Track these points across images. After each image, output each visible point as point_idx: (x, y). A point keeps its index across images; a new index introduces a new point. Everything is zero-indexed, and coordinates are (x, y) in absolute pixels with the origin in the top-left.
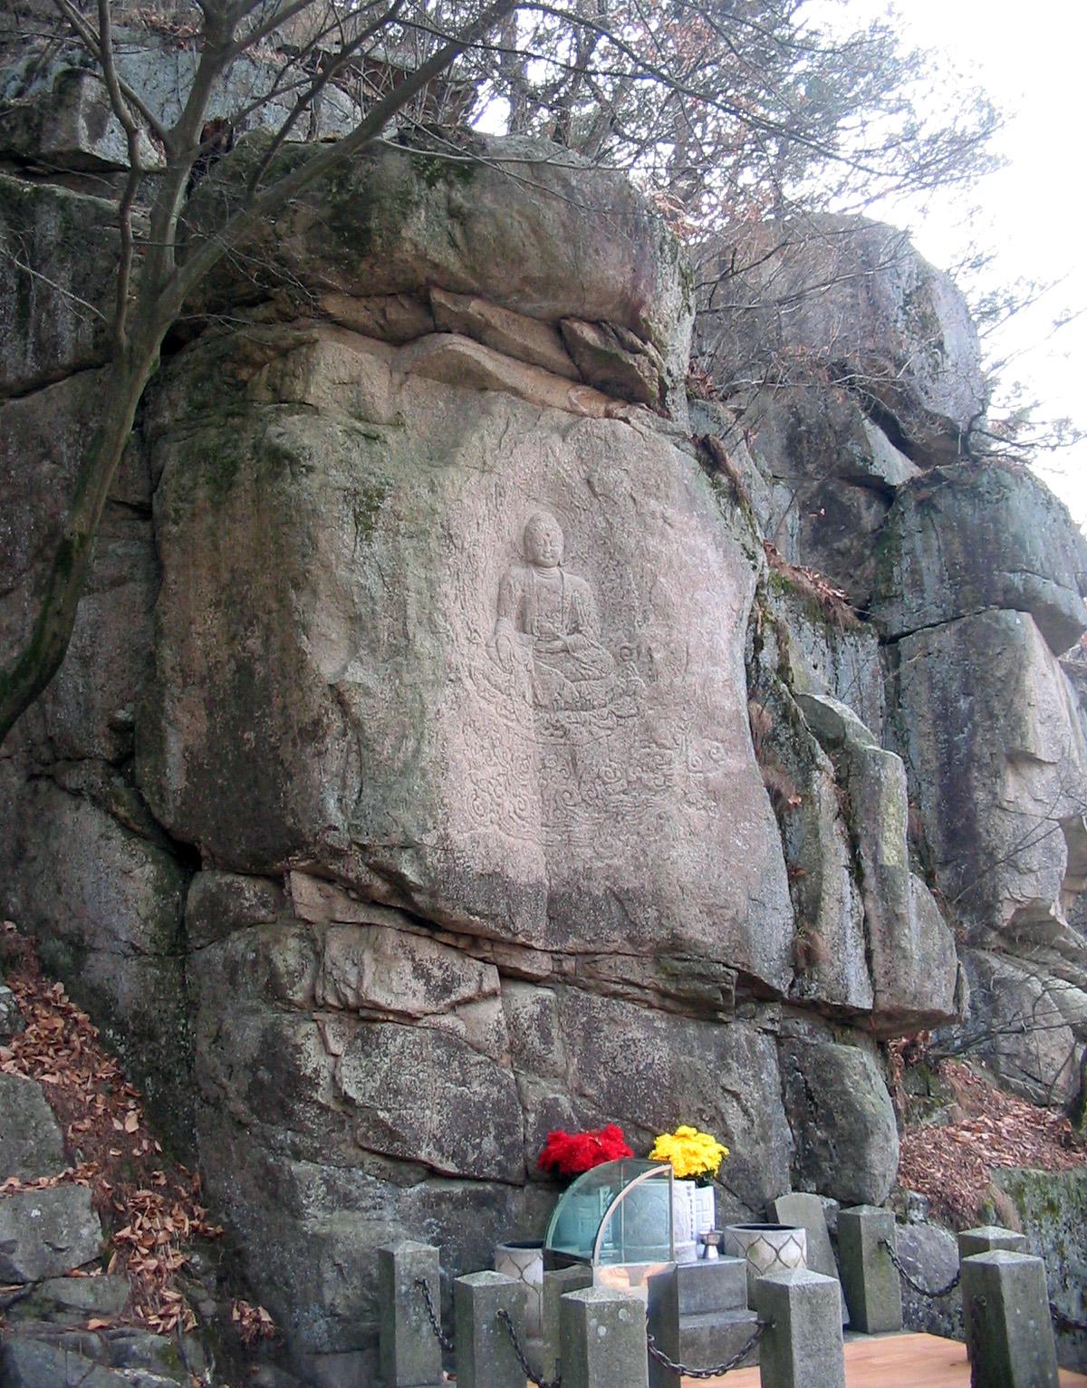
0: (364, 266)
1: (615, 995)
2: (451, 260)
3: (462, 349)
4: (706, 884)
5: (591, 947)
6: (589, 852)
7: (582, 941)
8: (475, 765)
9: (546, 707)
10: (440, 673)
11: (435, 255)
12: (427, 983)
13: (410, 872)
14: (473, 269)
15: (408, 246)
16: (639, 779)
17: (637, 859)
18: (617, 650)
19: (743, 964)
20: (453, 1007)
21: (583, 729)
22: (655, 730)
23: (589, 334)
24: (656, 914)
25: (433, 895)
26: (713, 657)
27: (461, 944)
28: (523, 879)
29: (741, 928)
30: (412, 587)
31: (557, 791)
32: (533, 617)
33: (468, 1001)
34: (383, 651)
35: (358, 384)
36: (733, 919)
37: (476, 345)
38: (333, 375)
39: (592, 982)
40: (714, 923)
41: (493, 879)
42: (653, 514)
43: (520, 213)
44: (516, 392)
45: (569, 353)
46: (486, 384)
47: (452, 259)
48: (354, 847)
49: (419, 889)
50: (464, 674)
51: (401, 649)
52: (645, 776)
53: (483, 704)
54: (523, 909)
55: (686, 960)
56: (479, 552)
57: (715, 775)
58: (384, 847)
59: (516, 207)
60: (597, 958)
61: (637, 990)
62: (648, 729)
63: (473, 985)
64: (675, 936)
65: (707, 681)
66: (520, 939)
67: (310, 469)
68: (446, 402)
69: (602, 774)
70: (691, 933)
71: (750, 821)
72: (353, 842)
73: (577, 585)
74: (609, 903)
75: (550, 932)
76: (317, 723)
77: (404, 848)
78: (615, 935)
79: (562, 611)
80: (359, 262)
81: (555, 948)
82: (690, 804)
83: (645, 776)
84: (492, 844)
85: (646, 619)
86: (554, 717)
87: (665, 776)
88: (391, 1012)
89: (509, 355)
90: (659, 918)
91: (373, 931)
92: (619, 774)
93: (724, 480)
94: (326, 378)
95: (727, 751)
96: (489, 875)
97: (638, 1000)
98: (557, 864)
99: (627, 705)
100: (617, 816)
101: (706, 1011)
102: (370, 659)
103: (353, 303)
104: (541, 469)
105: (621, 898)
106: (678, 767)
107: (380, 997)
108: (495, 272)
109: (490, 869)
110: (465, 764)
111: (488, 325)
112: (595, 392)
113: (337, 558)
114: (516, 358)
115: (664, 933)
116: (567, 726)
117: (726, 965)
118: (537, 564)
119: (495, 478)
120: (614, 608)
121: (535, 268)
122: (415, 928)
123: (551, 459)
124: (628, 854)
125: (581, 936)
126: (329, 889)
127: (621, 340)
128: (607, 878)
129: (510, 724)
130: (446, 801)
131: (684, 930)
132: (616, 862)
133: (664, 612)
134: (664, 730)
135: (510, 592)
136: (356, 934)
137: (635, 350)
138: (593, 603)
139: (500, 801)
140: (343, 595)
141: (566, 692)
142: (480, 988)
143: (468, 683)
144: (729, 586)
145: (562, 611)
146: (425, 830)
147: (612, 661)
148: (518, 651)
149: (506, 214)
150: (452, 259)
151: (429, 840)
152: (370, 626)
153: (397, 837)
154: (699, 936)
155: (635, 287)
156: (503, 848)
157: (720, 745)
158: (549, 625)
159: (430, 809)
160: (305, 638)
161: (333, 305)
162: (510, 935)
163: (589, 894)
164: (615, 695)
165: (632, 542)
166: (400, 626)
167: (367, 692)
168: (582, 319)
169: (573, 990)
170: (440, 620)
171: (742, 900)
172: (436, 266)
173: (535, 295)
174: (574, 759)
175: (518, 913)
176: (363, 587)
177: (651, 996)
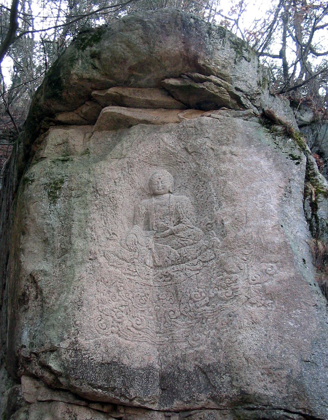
0: (64, 94)
2: (96, 75)
3: (110, 111)
4: (264, 354)
5: (187, 406)
6: (185, 345)
7: (182, 403)
8: (103, 302)
9: (161, 266)
11: (86, 75)
13: (54, 365)
14: (106, 75)
15: (74, 77)
16: (216, 295)
17: (215, 344)
18: (204, 227)
19: (304, 410)
21: (181, 273)
22: (226, 264)
23: (172, 81)
24: (229, 379)
25: (67, 377)
26: (265, 215)
27: (105, 409)
28: (137, 365)
29: (296, 382)
30: (76, 219)
31: (166, 312)
32: (153, 222)
34: (58, 253)
35: (67, 142)
36: (288, 376)
37: (119, 108)
38: (55, 142)
40: (274, 381)
41: (112, 367)
42: (224, 153)
43: (121, 42)
44: (146, 122)
45: (173, 97)
46: (130, 123)
47: (95, 74)
48: (33, 355)
51: (66, 250)
52: (219, 293)
53: (112, 269)
54: (136, 384)
55: (253, 409)
56: (117, 196)
57: (271, 284)
58: (43, 352)
59: (118, 40)
60: (192, 412)
62: (221, 265)
64: (243, 393)
65: (260, 230)
66: (136, 403)
67: (33, 181)
68: (112, 138)
69: (192, 297)
70: (254, 389)
71: (300, 308)
72: (31, 353)
73: (183, 200)
74: (197, 376)
75: (163, 399)
76: (24, 294)
77: (52, 351)
78: (203, 396)
79: (170, 214)
80: (61, 93)
81: (166, 408)
82: (252, 304)
83: (219, 293)
84: (110, 345)
85: (220, 205)
86: (165, 270)
87: (233, 290)
89: (140, 108)
90: (231, 382)
91: (53, 405)
92: (203, 295)
93: (279, 128)
94: (52, 145)
95: (279, 267)
96: (108, 364)
98: (166, 355)
99: (209, 254)
100: (202, 319)
102: (51, 258)
103: (71, 114)
104: (156, 150)
105: (206, 371)
106: (241, 283)
108: (115, 71)
109: (109, 360)
110: (95, 302)
111: (122, 96)
112: (195, 111)
113: (38, 215)
114: (146, 108)
115: (235, 391)
116: (172, 274)
117: (286, 410)
118: (155, 195)
119: (127, 160)
120: (202, 205)
121: (132, 62)
123: (162, 143)
124: (209, 342)
125: (181, 399)
126: (38, 384)
128: (196, 359)
129: (132, 278)
130: (78, 322)
131: (249, 388)
132: (202, 348)
133: (231, 199)
134: (231, 263)
135: (139, 212)
137: (202, 81)
138: (190, 206)
139: (120, 320)
140: (40, 231)
141: (172, 256)
143: (102, 260)
144: (277, 177)
145: (170, 214)
146: (62, 339)
147: (202, 233)
148: (141, 240)
149: (114, 45)
150: (95, 74)
151: (64, 345)
152: (51, 242)
153: (47, 346)
154: (261, 391)
155: (187, 50)
156: (120, 347)
157: (274, 265)
158: (162, 223)
159: (66, 327)
160: (22, 255)
161: (61, 117)
162: (127, 401)
163: (185, 371)
164: (202, 250)
165: (212, 169)
166: (68, 239)
167: (45, 274)
168: (167, 77)
170: (88, 231)
171: (295, 362)
172: (89, 80)
173: (140, 74)
174: (176, 291)
175: (132, 386)
176: (48, 225)
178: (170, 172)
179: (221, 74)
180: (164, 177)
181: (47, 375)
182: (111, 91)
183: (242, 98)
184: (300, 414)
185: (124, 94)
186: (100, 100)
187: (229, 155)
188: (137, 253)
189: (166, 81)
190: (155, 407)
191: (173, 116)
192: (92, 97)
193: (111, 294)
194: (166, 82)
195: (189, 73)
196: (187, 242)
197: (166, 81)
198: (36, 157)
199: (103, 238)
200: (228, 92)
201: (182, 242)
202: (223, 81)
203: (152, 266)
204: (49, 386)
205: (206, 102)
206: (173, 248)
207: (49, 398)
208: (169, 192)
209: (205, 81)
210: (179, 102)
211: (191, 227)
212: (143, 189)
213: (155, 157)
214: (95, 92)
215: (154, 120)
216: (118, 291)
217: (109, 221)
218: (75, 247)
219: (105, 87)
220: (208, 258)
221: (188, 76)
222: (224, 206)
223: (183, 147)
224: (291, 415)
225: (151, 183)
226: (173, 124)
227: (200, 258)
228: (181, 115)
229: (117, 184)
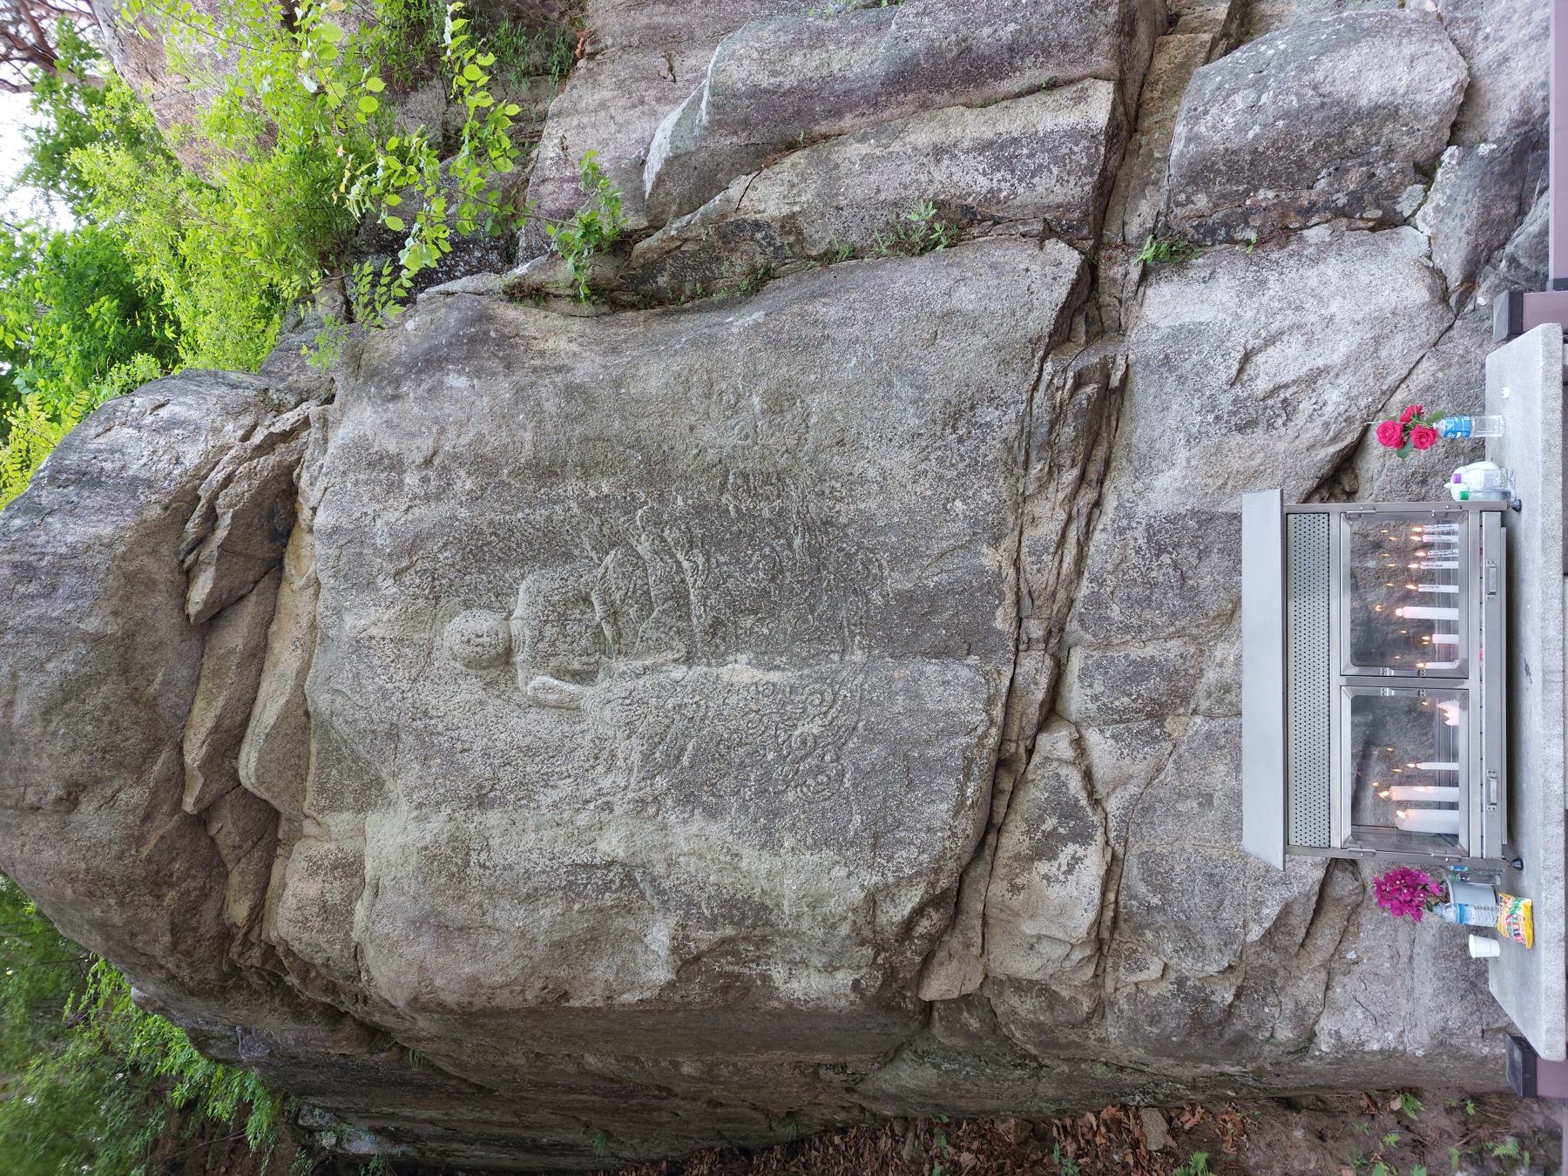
1: (1081, 557)
2: (134, 796)
5: (1010, 598)
12: (1064, 840)
20: (1096, 803)
23: (201, 591)
33: (1088, 775)
39: (1061, 595)
45: (242, 597)
49: (932, 885)
60: (1024, 590)
61: (1074, 527)
63: (1064, 771)
88: (1104, 894)
91: (993, 912)
97: (1088, 524)
101: (1107, 405)
107: (1083, 920)
111: (216, 729)
114: (260, 671)
117: (1035, 388)
118: (509, 652)
122: (987, 852)
127: (200, 542)
136: (996, 933)
142: (1067, 763)
158: (583, 643)
161: (239, 911)
162: (993, 731)
169: (1073, 626)
177: (1086, 497)
178: (451, 617)
179: (197, 468)
180: (467, 627)
181: (924, 926)
182: (194, 753)
183: (272, 429)
184: (1043, 360)
185: (209, 724)
186: (215, 787)
189: (192, 609)
190: (1007, 672)
191: (296, 601)
192: (198, 816)
194: (199, 607)
195: (183, 546)
197: (192, 609)
198: (347, 978)
200: (251, 459)
202: (220, 466)
204: (952, 923)
205: (272, 514)
207: (978, 923)
208: (506, 619)
209: (214, 510)
210: (261, 585)
214: (189, 805)
216: (740, 744)
218: (621, 854)
219: (178, 778)
221: (189, 552)
223: (390, 582)
224: (1046, 377)
226: (320, 603)
228: (299, 583)
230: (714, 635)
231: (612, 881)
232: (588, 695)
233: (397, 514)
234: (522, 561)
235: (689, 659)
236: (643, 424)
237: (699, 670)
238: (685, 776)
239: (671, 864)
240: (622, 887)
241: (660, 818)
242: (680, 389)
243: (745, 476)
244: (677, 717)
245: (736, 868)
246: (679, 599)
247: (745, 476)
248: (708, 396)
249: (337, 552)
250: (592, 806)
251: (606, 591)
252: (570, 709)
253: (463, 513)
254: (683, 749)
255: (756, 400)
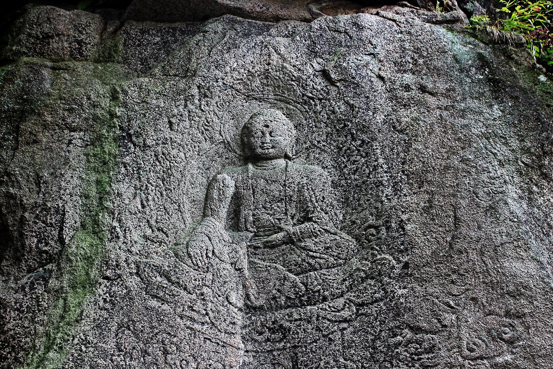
9: (261, 308)
10: (94, 273)
50: (125, 271)
123: (275, 57)
129: (196, 326)
147: (353, 244)
148: (225, 251)
158: (266, 217)
180: (280, 127)
187: (415, 93)
188: (209, 276)
193: (149, 359)
196: (322, 261)
199: (136, 236)
201: (312, 261)
203: (240, 304)
206: (290, 271)
208: (286, 157)
211: (329, 228)
212: (226, 144)
213: (257, 82)
215: (258, 9)
216: (166, 353)
217: (151, 203)
220: (365, 298)
222: (405, 191)
225: (247, 131)
226: (298, 23)
227: (351, 295)
229: (175, 127)
230: (272, 331)
231: (47, 244)
232: (218, 225)
233: (376, 70)
234: (339, 167)
235: (249, 308)
236: (474, 256)
237: (239, 318)
238: (137, 302)
239: (58, 292)
240: (41, 252)
241: (101, 280)
242: (511, 288)
243: (430, 350)
244: (194, 296)
245: (48, 349)
246: (312, 297)
247: (430, 350)
248: (508, 314)
249: (342, 29)
250: (116, 224)
251: (313, 235)
252: (206, 209)
253: (380, 118)
254: (163, 300)
255: (508, 357)
